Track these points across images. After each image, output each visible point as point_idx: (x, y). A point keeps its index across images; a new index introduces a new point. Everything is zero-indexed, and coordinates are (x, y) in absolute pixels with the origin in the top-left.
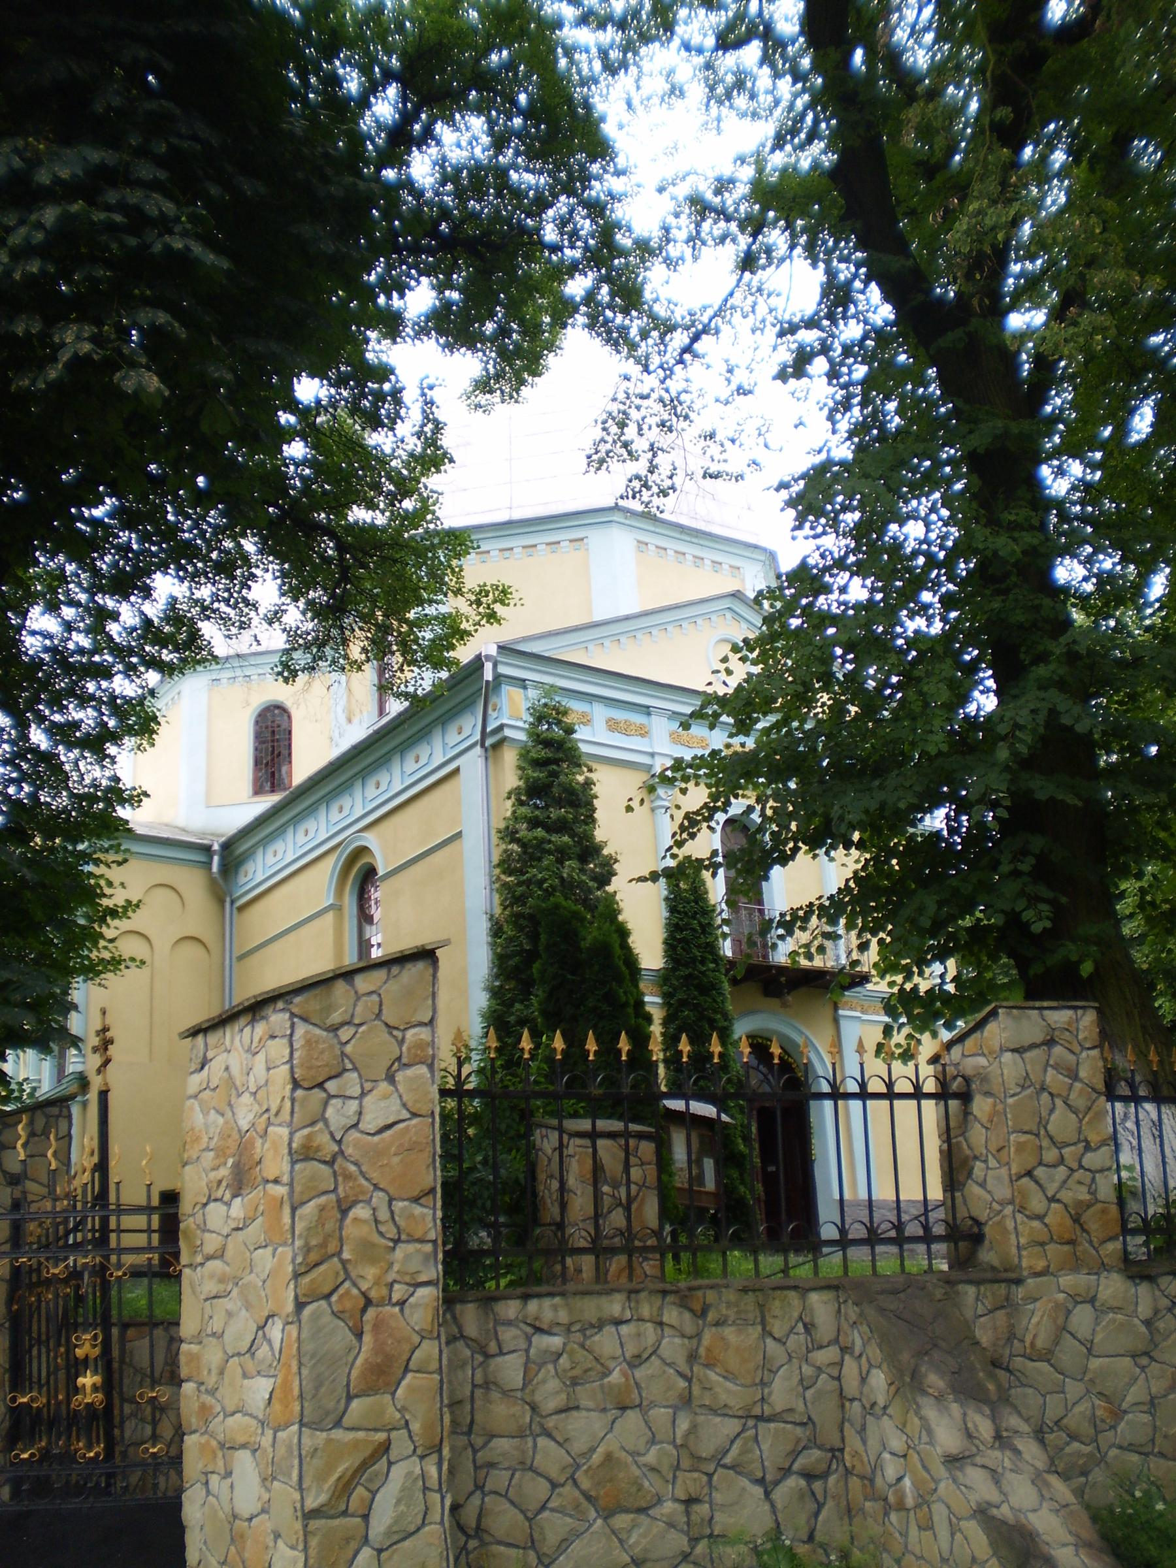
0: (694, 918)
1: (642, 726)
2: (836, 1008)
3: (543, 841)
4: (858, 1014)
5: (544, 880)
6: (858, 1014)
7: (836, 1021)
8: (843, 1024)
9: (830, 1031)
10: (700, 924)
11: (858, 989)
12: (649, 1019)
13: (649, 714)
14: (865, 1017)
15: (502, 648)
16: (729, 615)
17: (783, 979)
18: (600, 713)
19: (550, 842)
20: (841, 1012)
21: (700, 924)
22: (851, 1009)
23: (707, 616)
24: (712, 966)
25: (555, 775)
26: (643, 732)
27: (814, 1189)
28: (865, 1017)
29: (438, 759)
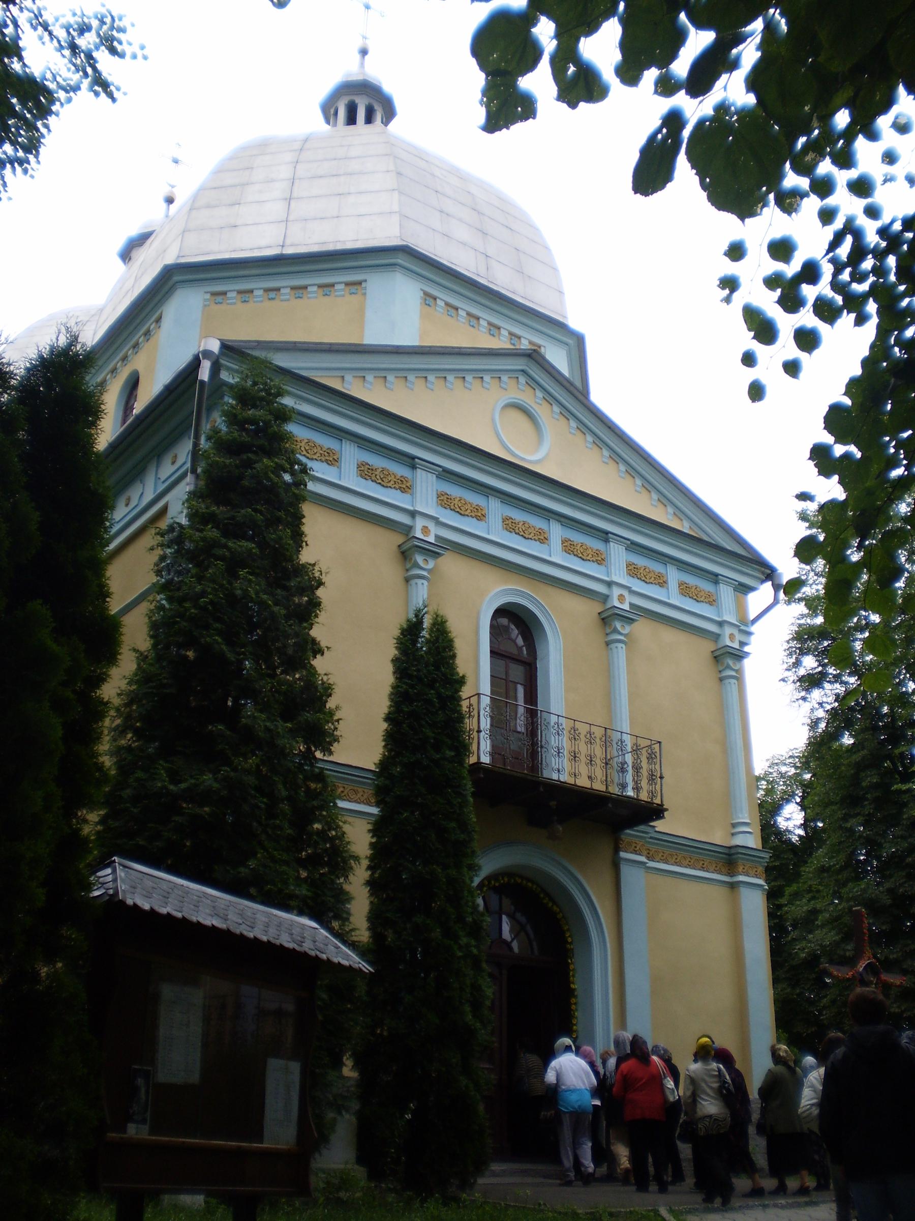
0: (431, 686)
1: (403, 480)
2: (617, 850)
3: (214, 544)
4: (643, 859)
5: (203, 594)
6: (643, 859)
7: (616, 866)
8: (625, 870)
9: (607, 877)
10: (439, 696)
11: (642, 828)
12: (103, 639)
13: (414, 467)
14: (651, 864)
15: (226, 347)
16: (522, 380)
17: (553, 803)
18: (351, 455)
19: (225, 546)
20: (623, 854)
21: (439, 696)
22: (635, 852)
23: (497, 374)
24: (450, 753)
25: (249, 464)
26: (405, 487)
27: (633, 183)
28: (651, 864)
29: (149, 496)
